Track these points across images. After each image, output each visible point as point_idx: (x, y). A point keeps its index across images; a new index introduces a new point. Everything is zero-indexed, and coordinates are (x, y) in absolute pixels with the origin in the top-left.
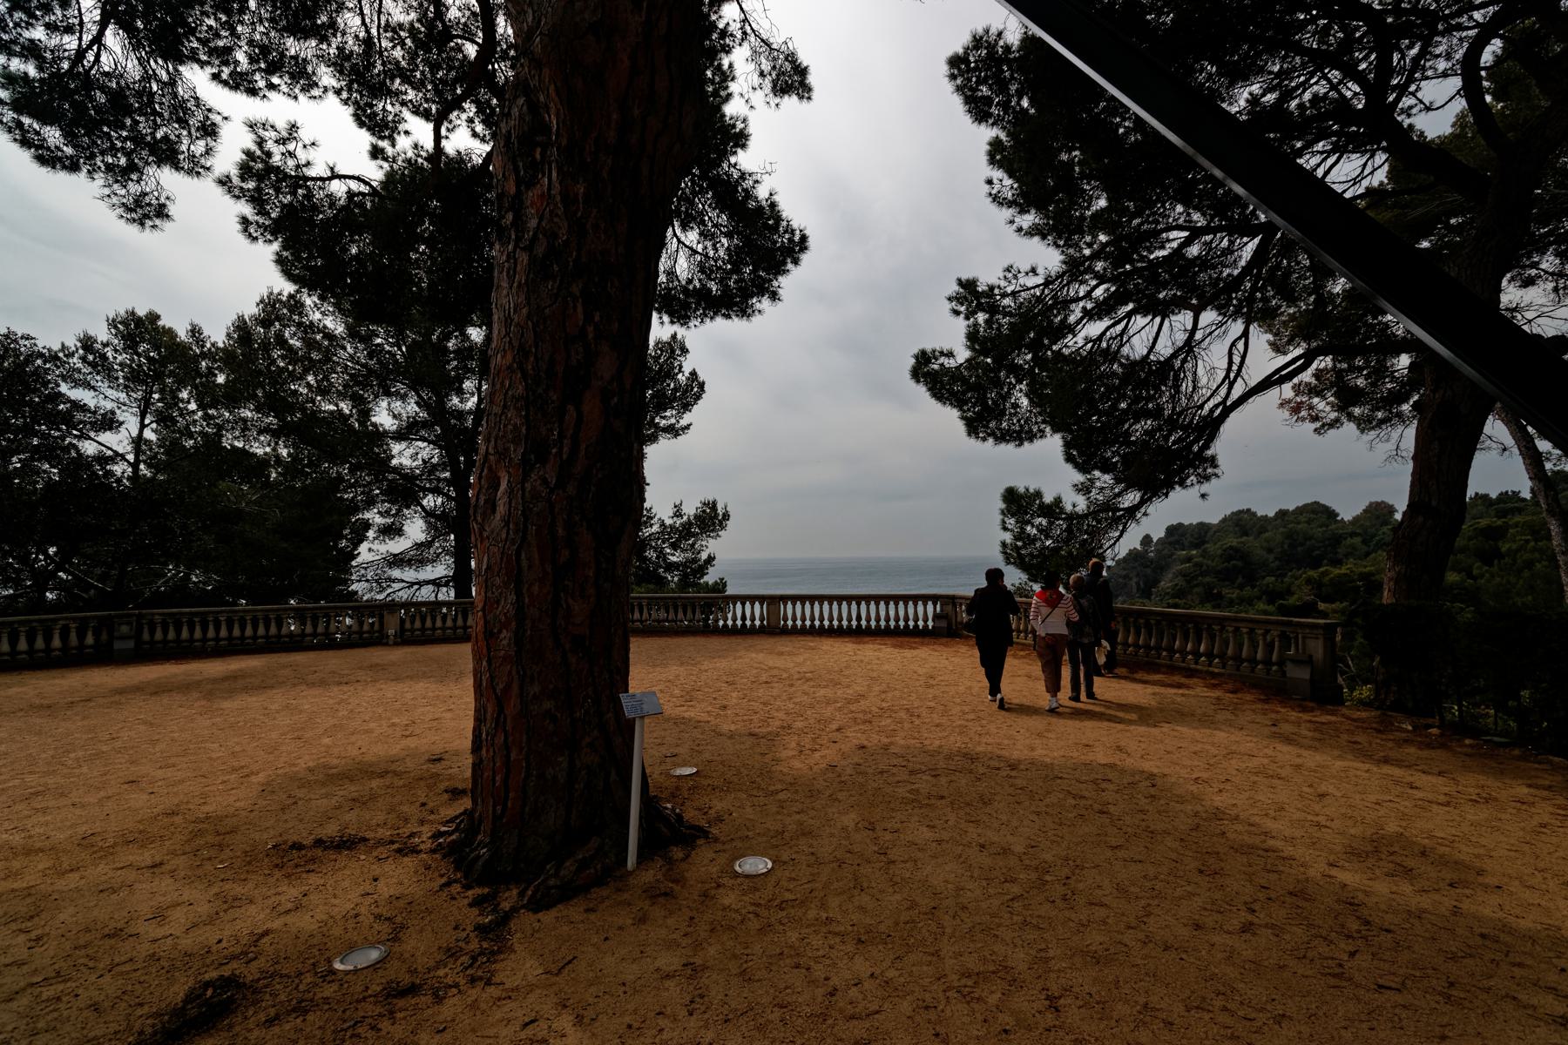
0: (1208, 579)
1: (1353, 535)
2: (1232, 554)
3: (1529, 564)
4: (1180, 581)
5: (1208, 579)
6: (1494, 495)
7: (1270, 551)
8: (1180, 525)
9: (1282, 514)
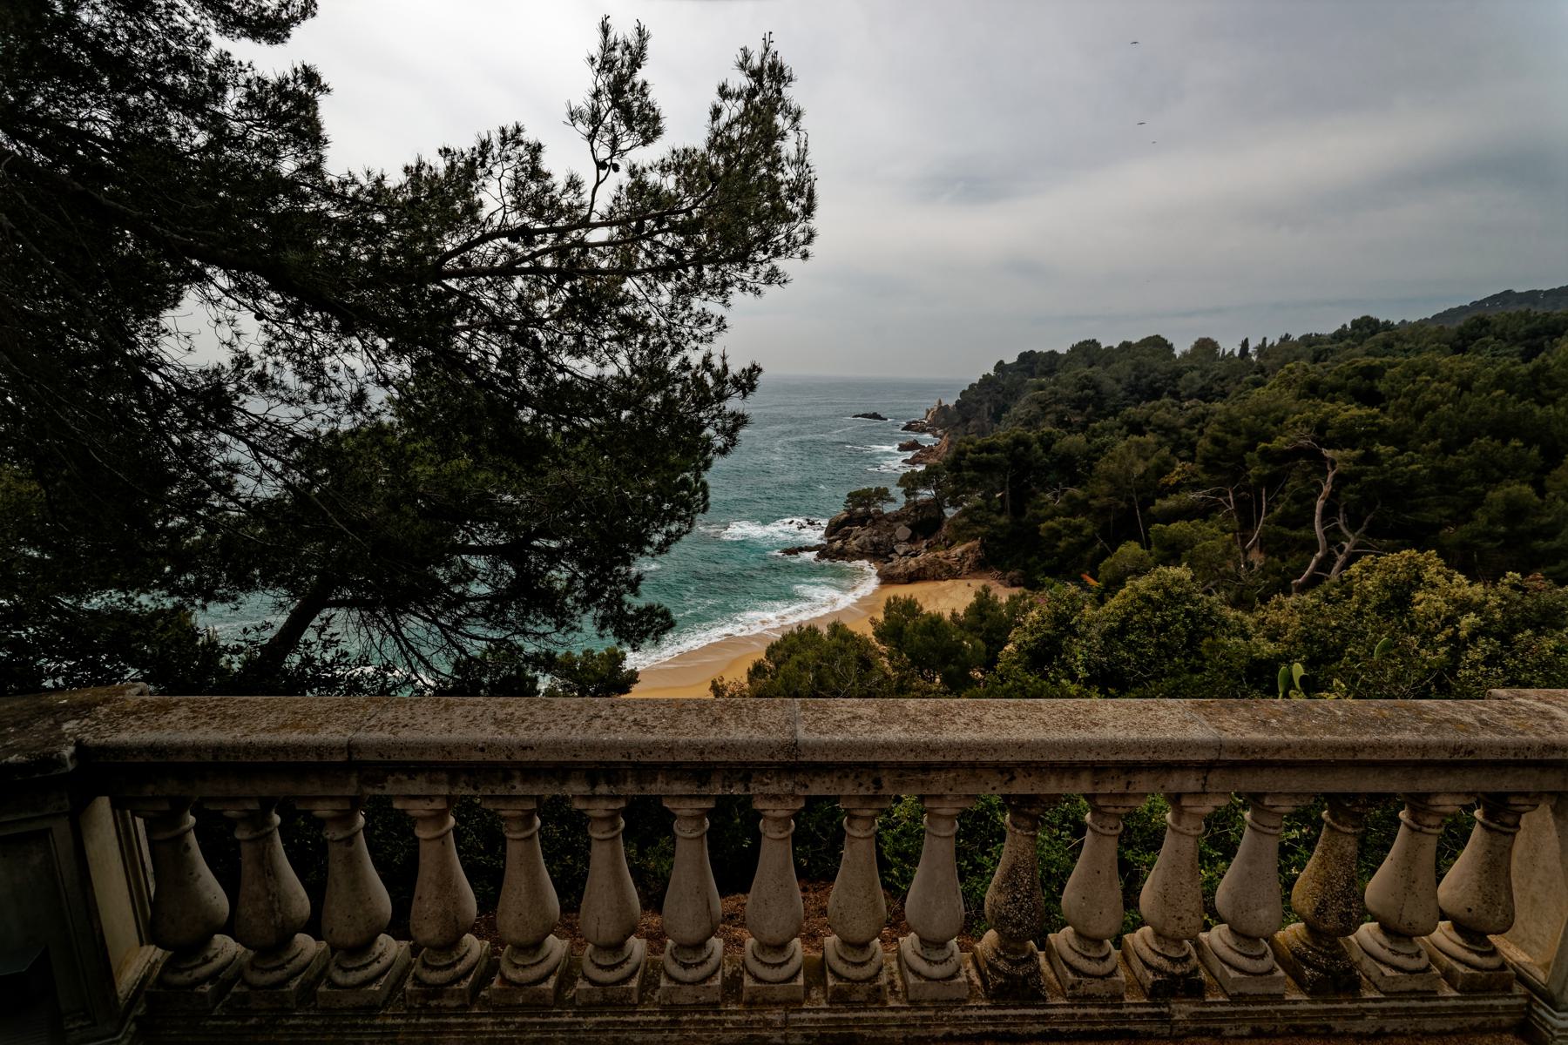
0: (1061, 407)
1: (1192, 368)
2: (1087, 383)
3: (1432, 406)
4: (1035, 409)
5: (1061, 407)
7: (1118, 381)
8: (1032, 352)
9: (1126, 346)
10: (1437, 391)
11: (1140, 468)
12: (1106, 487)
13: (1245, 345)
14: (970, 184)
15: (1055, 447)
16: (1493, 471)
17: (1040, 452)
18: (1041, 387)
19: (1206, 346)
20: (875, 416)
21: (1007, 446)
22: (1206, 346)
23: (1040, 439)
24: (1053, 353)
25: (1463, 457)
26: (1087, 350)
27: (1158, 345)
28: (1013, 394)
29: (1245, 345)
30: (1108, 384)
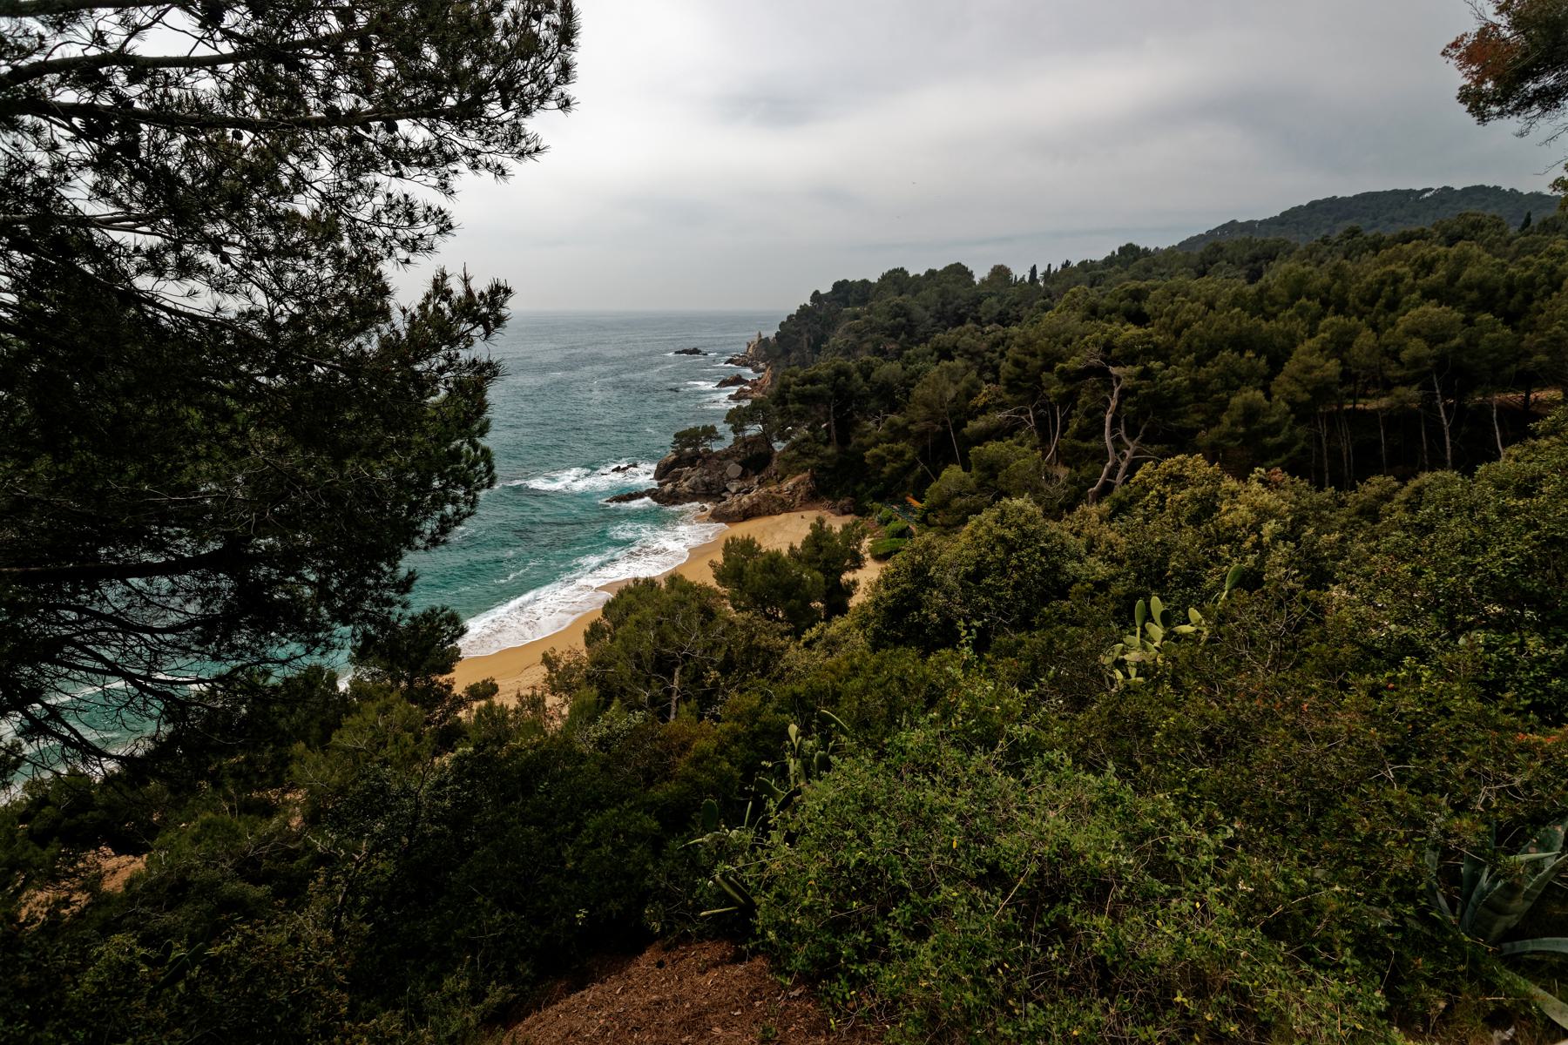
1: (990, 295)
2: (901, 311)
3: (1187, 324)
4: (852, 338)
5: (876, 335)
6: (874, 279)
7: (927, 308)
10: (1190, 311)
11: (951, 393)
12: (922, 412)
13: (1034, 271)
14: (775, 106)
15: (874, 375)
16: (1234, 380)
17: (861, 381)
18: (857, 317)
19: (1000, 273)
20: (696, 351)
21: (829, 376)
22: (1000, 273)
23: (860, 369)
24: (865, 282)
25: (1211, 369)
26: (896, 279)
27: (959, 272)
28: (830, 324)
29: (1034, 271)
30: (918, 311)
